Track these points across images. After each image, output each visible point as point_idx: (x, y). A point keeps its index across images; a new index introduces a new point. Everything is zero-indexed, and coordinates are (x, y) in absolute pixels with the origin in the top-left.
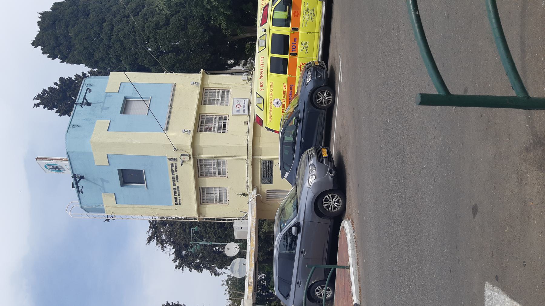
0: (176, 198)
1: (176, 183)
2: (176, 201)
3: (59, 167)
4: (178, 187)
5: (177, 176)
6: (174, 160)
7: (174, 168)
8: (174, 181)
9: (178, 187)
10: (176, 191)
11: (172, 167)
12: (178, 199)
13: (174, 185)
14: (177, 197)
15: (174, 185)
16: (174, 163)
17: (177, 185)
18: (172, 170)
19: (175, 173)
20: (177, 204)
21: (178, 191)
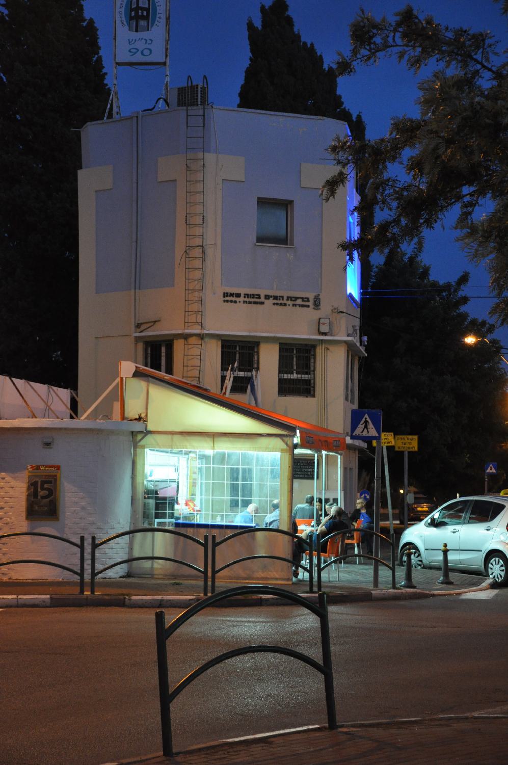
0: (238, 295)
2: (232, 295)
3: (143, 23)
4: (262, 303)
5: (285, 305)
6: (317, 304)
7: (299, 302)
8: (275, 298)
10: (254, 299)
11: (302, 299)
12: (238, 299)
13: (267, 297)
14: (242, 299)
15: (267, 297)
16: (311, 303)
17: (266, 302)
18: (296, 298)
19: (289, 302)
20: (226, 295)
21: (255, 303)
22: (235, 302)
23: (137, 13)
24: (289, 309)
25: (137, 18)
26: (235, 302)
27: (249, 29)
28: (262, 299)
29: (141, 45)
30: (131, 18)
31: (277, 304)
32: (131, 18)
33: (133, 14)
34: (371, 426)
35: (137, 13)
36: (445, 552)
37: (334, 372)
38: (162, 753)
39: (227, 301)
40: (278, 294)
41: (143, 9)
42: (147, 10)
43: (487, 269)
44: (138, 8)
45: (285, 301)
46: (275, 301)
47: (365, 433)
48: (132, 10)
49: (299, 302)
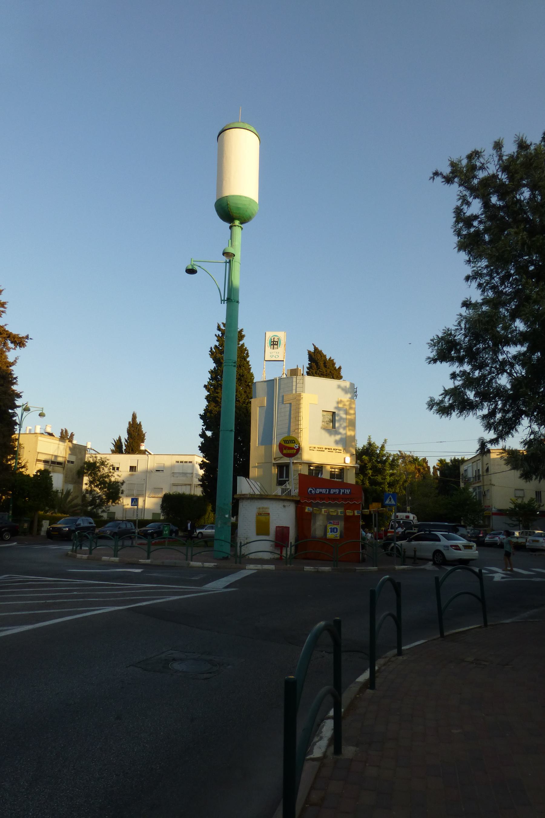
0: (315, 448)
3: (275, 346)
7: (338, 451)
8: (329, 449)
13: (326, 449)
14: (316, 449)
15: (326, 449)
19: (334, 451)
24: (334, 454)
25: (274, 344)
27: (217, 355)
28: (324, 449)
29: (274, 354)
34: (392, 500)
36: (415, 551)
37: (120, 492)
38: (439, 636)
42: (277, 342)
43: (99, 457)
44: (274, 341)
47: (390, 503)
49: (338, 451)
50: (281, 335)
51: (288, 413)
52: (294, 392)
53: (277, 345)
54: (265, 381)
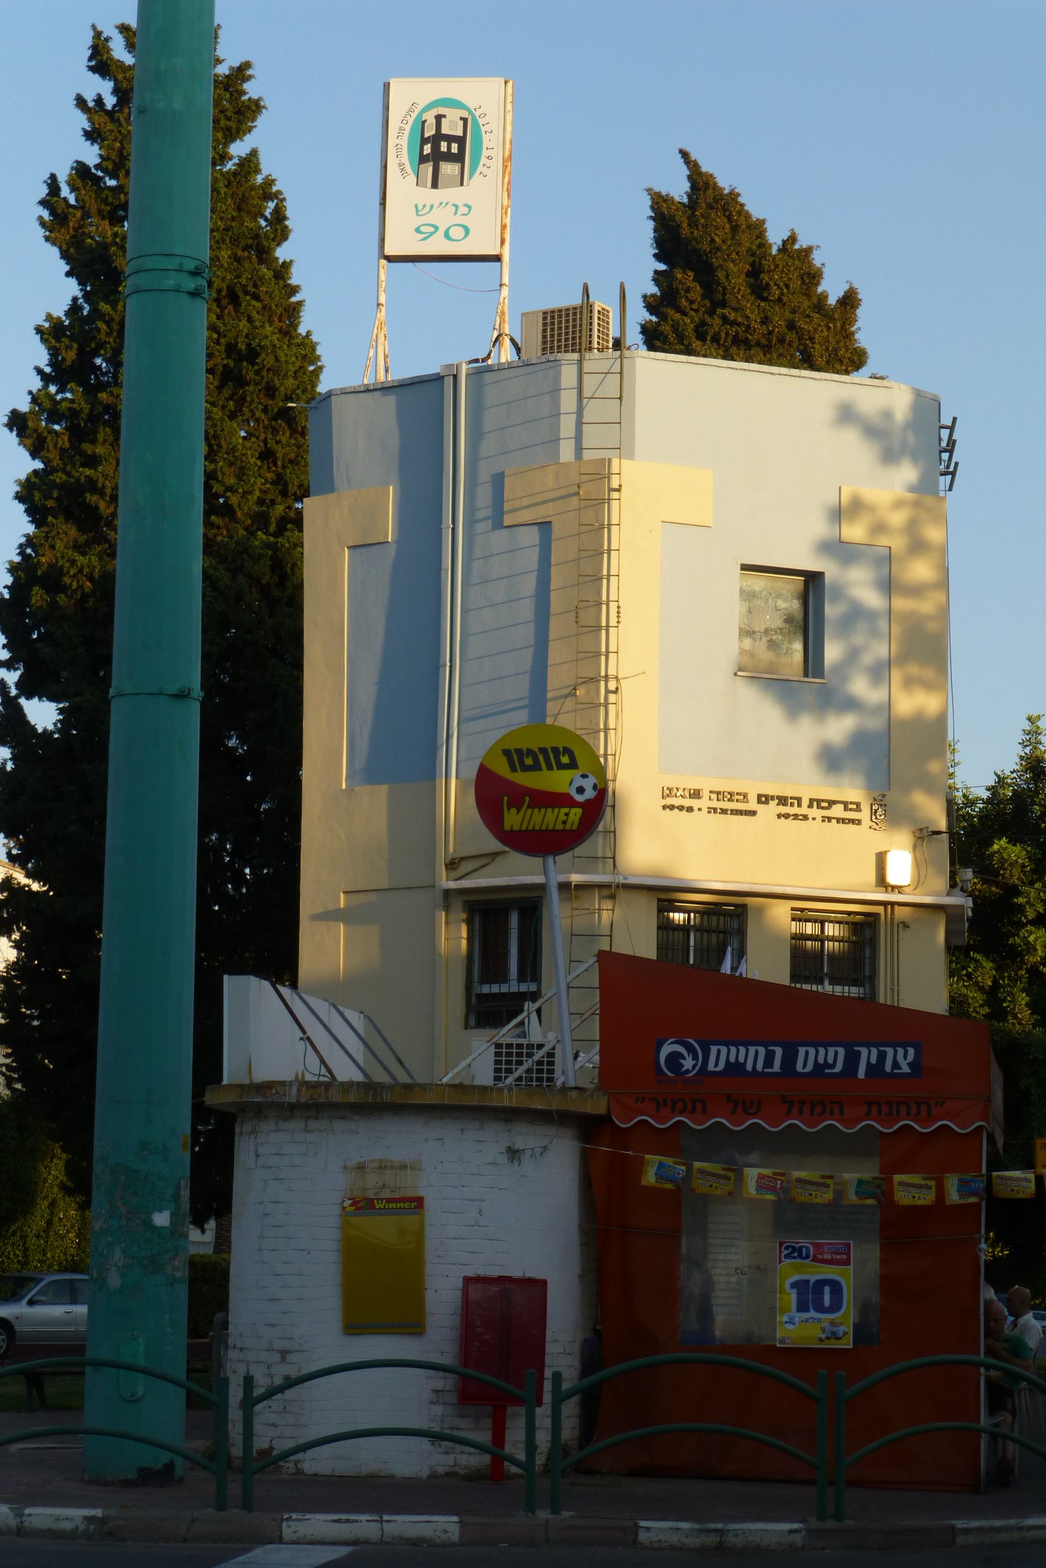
0: (696, 794)
1: (773, 807)
3: (448, 169)
4: (753, 813)
5: (805, 817)
8: (783, 801)
9: (753, 813)
13: (764, 799)
14: (704, 803)
15: (764, 799)
17: (760, 809)
19: (815, 812)
22: (690, 809)
23: (436, 147)
26: (690, 809)
28: (752, 805)
30: (423, 159)
31: (787, 816)
32: (423, 159)
33: (427, 149)
35: (436, 147)
39: (672, 807)
40: (788, 792)
41: (450, 139)
42: (461, 141)
44: (439, 137)
45: (804, 810)
46: (783, 810)
48: (424, 141)
50: (484, 99)
51: (529, 585)
52: (566, 452)
53: (459, 158)
54: (385, 389)
